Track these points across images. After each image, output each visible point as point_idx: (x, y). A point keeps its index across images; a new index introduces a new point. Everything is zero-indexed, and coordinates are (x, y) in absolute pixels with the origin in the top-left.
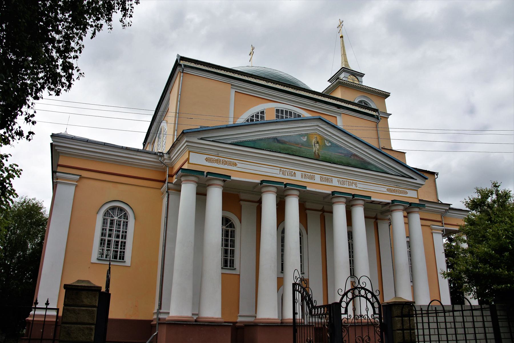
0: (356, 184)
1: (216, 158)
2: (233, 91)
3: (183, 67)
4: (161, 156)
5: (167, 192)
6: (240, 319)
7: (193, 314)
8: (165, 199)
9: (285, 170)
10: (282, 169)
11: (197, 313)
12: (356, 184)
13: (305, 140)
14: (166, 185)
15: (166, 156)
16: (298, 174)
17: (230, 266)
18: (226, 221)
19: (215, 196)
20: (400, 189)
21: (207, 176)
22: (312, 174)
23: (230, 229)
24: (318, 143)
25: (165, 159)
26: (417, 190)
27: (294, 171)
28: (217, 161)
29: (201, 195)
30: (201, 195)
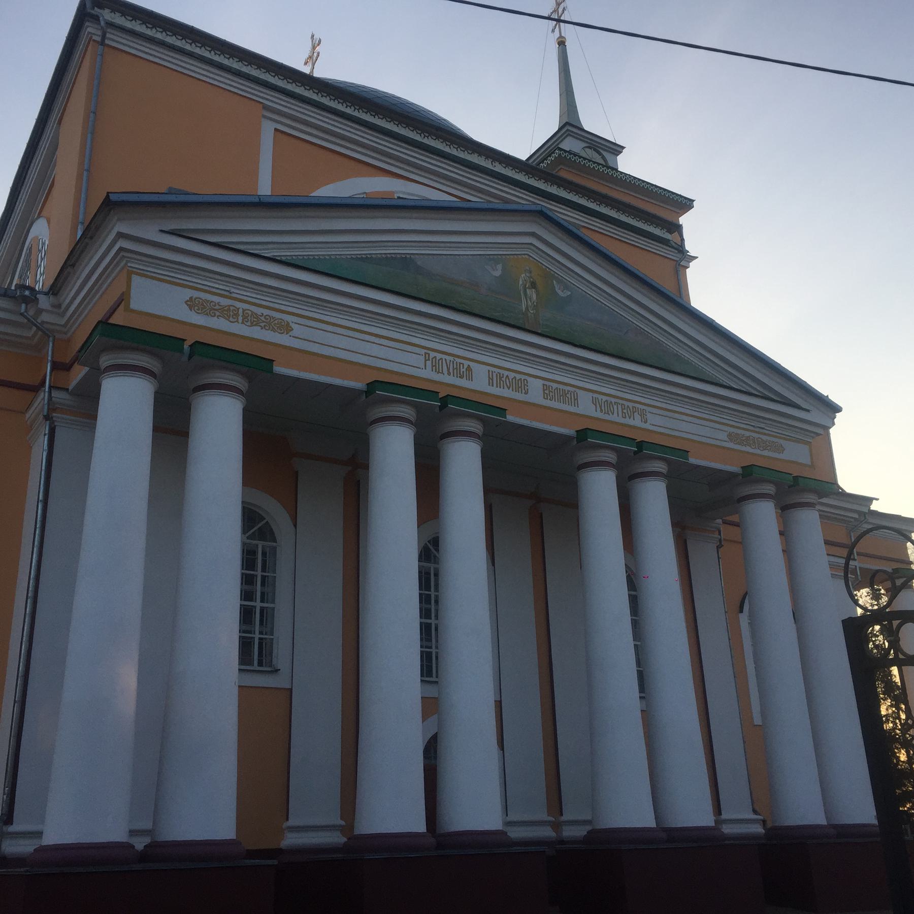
0: (643, 414)
1: (225, 302)
2: (268, 129)
3: (102, 23)
4: (26, 300)
5: (47, 418)
6: (290, 840)
7: (508, 824)
8: (43, 442)
9: (439, 356)
10: (432, 354)
11: (589, 818)
12: (643, 414)
13: (498, 273)
14: (43, 396)
15: (44, 302)
16: (481, 372)
17: (260, 664)
18: (251, 517)
19: (220, 424)
20: (764, 438)
21: (190, 357)
22: (518, 376)
23: (260, 544)
24: (533, 285)
25: (40, 311)
26: (808, 443)
27: (466, 363)
28: (228, 313)
29: (172, 427)
30: (172, 427)
